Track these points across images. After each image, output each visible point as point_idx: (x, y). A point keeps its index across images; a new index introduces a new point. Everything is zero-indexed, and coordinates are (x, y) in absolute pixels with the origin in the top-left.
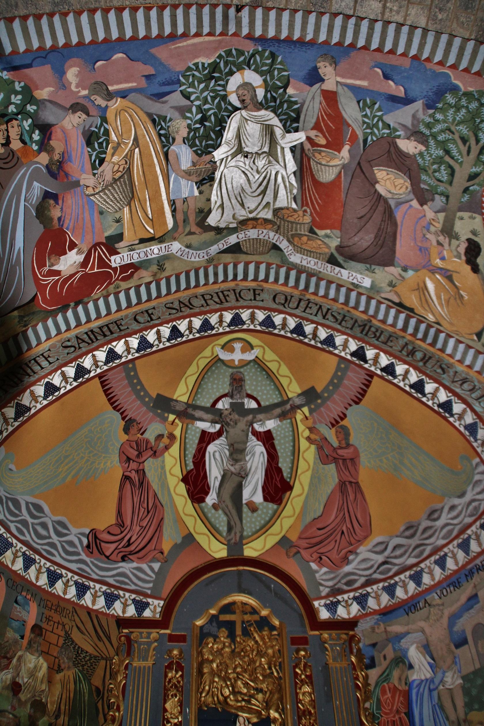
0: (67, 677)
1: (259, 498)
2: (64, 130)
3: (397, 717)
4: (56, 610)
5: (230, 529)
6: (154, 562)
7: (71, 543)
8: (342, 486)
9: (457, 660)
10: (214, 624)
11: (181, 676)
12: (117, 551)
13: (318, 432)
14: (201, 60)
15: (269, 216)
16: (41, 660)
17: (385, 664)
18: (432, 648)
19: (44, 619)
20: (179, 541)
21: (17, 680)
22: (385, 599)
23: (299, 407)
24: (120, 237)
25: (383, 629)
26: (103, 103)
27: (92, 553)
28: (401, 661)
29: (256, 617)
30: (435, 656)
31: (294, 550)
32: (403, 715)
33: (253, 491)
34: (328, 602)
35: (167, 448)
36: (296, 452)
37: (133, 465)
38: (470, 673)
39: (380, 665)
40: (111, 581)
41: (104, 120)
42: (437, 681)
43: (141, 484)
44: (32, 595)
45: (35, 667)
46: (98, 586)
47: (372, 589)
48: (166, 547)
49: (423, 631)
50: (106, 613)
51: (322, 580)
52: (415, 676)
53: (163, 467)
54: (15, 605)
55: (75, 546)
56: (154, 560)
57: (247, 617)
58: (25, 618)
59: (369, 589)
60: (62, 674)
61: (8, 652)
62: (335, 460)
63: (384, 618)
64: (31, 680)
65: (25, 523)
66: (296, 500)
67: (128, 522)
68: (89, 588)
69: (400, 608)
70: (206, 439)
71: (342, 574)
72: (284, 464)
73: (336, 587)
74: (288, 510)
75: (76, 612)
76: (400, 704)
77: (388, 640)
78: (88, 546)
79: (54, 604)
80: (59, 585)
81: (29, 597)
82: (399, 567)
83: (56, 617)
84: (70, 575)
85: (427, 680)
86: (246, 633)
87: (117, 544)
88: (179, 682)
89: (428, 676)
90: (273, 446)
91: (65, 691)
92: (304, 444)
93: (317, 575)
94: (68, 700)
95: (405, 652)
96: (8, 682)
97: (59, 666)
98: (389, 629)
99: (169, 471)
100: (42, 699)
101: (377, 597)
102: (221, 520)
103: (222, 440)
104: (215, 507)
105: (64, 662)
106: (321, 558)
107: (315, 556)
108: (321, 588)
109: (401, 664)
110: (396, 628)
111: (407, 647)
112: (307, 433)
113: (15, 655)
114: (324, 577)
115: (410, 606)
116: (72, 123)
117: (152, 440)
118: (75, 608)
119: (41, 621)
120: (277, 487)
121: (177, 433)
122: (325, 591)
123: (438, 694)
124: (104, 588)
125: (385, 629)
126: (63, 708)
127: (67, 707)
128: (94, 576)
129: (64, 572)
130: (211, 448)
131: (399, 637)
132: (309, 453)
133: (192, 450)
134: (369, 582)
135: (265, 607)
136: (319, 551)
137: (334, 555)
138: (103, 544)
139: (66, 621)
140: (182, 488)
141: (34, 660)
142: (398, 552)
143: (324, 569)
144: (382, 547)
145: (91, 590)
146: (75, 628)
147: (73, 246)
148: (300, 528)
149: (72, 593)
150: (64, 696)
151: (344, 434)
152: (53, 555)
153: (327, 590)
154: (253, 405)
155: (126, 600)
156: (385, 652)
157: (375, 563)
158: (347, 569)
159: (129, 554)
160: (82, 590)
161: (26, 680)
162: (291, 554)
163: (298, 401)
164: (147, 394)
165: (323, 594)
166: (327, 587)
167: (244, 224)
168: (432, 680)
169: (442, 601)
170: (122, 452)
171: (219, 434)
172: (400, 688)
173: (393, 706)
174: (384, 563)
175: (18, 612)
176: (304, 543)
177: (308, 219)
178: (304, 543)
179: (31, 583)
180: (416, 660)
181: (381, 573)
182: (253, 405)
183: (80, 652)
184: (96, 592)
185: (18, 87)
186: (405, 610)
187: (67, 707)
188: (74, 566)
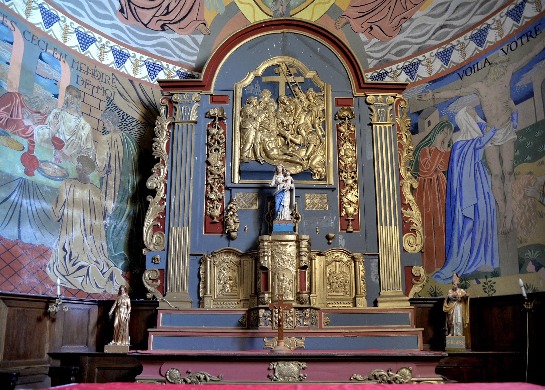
0: (114, 139)
3: (435, 176)
4: (93, 75)
6: (197, 34)
9: (515, 116)
10: (258, 86)
11: (224, 133)
12: (155, 19)
16: (83, 121)
17: (428, 130)
18: (485, 108)
19: (80, 82)
20: (222, 11)
21: (57, 135)
25: (431, 97)
27: (127, 18)
29: (301, 79)
30: (487, 116)
31: (343, 20)
32: (442, 173)
34: (375, 74)
38: (530, 127)
39: (424, 129)
40: (152, 50)
42: (484, 140)
44: (61, 55)
45: (77, 126)
46: (138, 55)
47: (424, 56)
48: (209, 17)
49: (477, 93)
50: (150, 83)
51: (371, 52)
54: (40, 61)
55: (106, 9)
56: (197, 31)
57: (291, 79)
58: (57, 78)
59: (420, 57)
60: (108, 136)
61: (41, 108)
63: (434, 85)
64: (74, 138)
68: (128, 56)
69: (453, 73)
71: (395, 42)
73: (385, 58)
75: (117, 80)
76: (439, 164)
77: (435, 106)
78: (122, 11)
79: (90, 69)
81: (58, 56)
82: (460, 28)
83: (95, 82)
84: (104, 40)
85: (473, 140)
86: (290, 93)
87: (154, 11)
88: (222, 138)
89: (476, 136)
91: (113, 151)
93: (366, 47)
94: (117, 159)
96: (47, 137)
97: (104, 128)
98: (437, 95)
100: (89, 156)
105: (109, 125)
106: (371, 28)
107: (366, 26)
108: (369, 60)
109: (446, 128)
111: (455, 111)
113: (50, 112)
114: (373, 49)
115: (466, 70)
118: (116, 76)
119: (77, 83)
122: (372, 63)
123: (484, 151)
124: (145, 58)
125: (433, 95)
126: (113, 165)
127: (117, 165)
128: (133, 45)
129: (97, 36)
131: (448, 102)
134: (421, 51)
135: (311, 70)
136: (369, 21)
137: (386, 25)
138: (137, 9)
139: (106, 86)
141: (74, 120)
142: (461, 12)
143: (375, 40)
145: (132, 59)
146: (117, 94)
149: (109, 59)
150: (113, 155)
152: (80, 15)
153: (375, 62)
155: (170, 71)
156: (430, 118)
157: (432, 28)
158: (399, 38)
159: (169, 23)
160: (121, 58)
161: (68, 137)
162: (340, 25)
165: (370, 67)
166: (376, 59)
168: (479, 140)
169: (507, 56)
172: (442, 150)
173: (431, 167)
174: (442, 27)
175: (45, 69)
176: (354, 13)
179: (56, 41)
180: (464, 122)
181: (436, 39)
183: (125, 117)
184: (137, 61)
186: (458, 74)
187: (117, 165)
188: (108, 31)
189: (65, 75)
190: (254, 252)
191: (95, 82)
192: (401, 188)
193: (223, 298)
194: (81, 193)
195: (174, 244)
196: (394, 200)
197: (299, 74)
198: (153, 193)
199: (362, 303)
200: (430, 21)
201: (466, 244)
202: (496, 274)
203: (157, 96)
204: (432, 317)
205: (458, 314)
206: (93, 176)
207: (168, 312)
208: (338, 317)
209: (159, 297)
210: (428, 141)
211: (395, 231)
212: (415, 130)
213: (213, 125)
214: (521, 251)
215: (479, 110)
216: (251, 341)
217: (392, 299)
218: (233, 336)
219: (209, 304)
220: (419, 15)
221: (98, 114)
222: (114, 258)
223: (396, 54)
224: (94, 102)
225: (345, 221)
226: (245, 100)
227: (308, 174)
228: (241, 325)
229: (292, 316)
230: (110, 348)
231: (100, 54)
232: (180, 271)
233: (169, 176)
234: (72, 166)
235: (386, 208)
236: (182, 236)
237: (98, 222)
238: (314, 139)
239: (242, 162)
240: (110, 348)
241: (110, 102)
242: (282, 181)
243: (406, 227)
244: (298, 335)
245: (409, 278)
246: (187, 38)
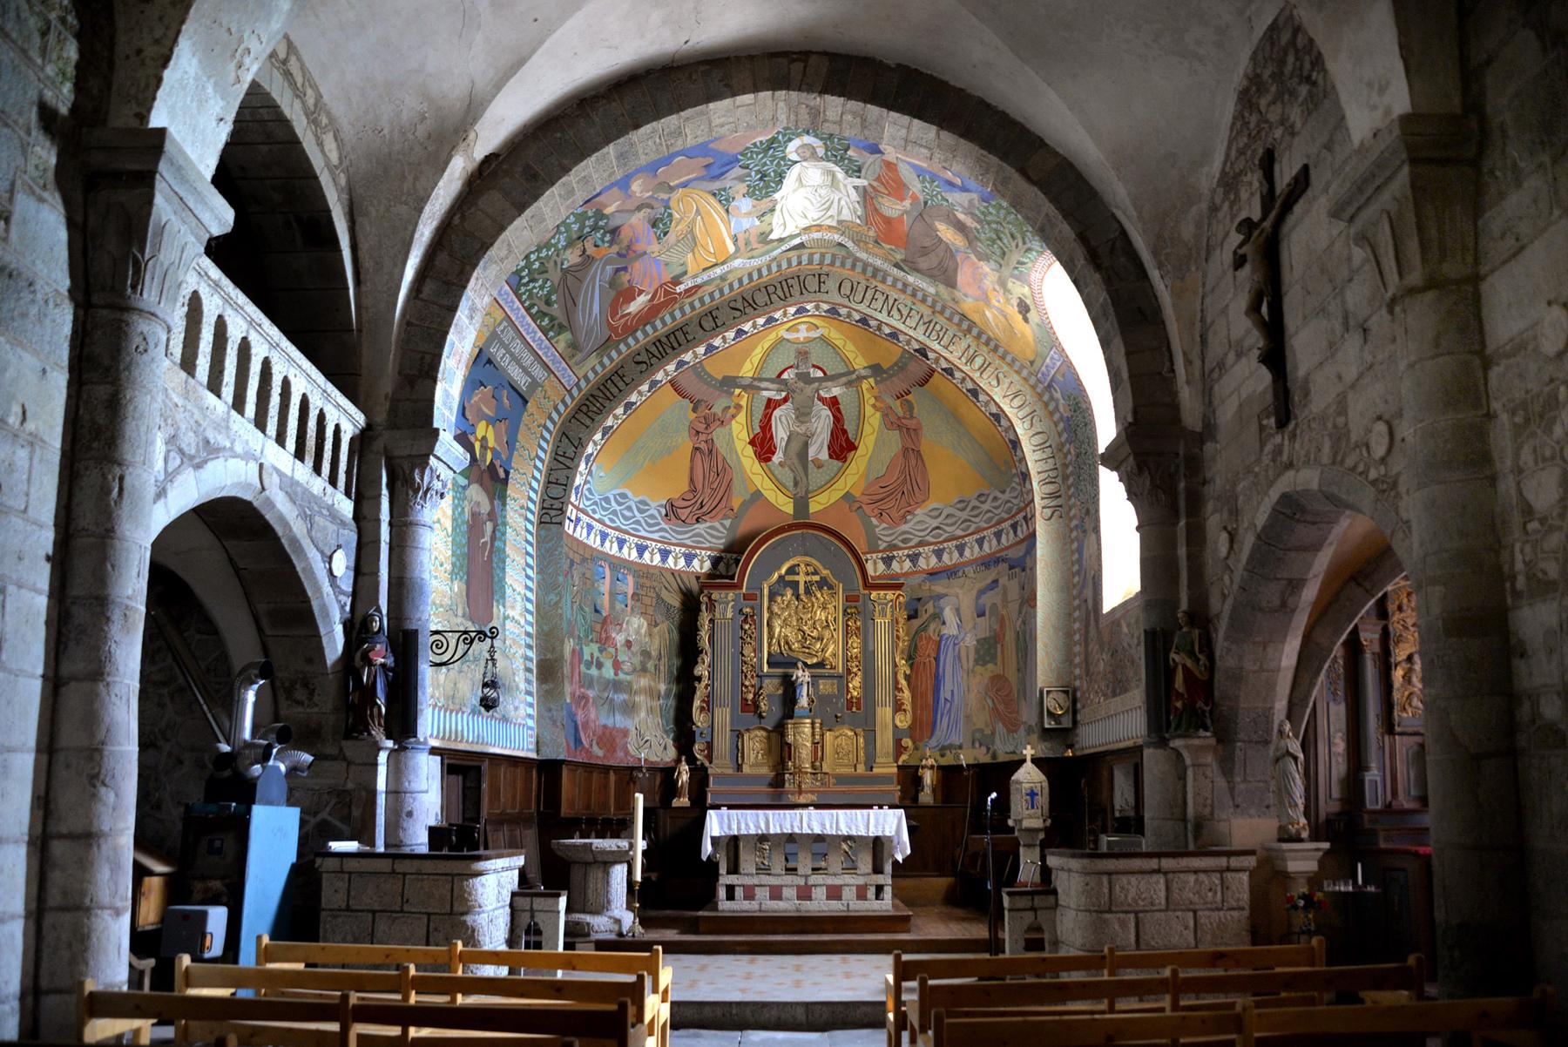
1: (824, 455)
2: (631, 226)
5: (796, 484)
7: (652, 517)
8: (905, 450)
13: (884, 402)
14: (757, 140)
15: (834, 224)
17: (925, 617)
20: (748, 497)
22: (933, 560)
23: (865, 378)
24: (685, 273)
26: (665, 197)
28: (937, 616)
29: (817, 578)
33: (819, 450)
35: (734, 416)
36: (861, 417)
37: (703, 437)
40: (688, 542)
41: (667, 207)
43: (710, 452)
48: (736, 503)
52: (945, 631)
53: (730, 434)
56: (725, 517)
62: (899, 427)
65: (614, 513)
66: (859, 463)
67: (699, 487)
70: (771, 405)
72: (849, 426)
74: (853, 468)
80: (647, 555)
83: (648, 583)
86: (808, 592)
90: (839, 410)
92: (869, 410)
95: (942, 610)
99: (739, 432)
101: (927, 559)
102: (787, 476)
103: (789, 404)
104: (781, 464)
107: (877, 512)
110: (938, 588)
112: (872, 401)
115: (951, 572)
116: (638, 220)
117: (719, 413)
120: (842, 446)
121: (743, 403)
122: (883, 546)
130: (777, 413)
131: (940, 597)
132: (874, 420)
133: (758, 415)
134: (921, 544)
137: (894, 513)
140: (750, 450)
142: (949, 521)
144: (935, 513)
147: (641, 292)
148: (863, 486)
151: (910, 407)
154: (820, 374)
158: (904, 527)
160: (665, 554)
163: (864, 373)
164: (713, 378)
167: (807, 229)
170: (691, 428)
171: (785, 400)
176: (866, 499)
177: (872, 233)
178: (866, 499)
182: (820, 374)
185: (590, 214)
189: (629, 586)
190: (780, 729)
191: (648, 583)
192: (895, 674)
193: (756, 765)
194: (644, 682)
195: (716, 721)
196: (889, 684)
197: (816, 573)
198: (699, 679)
199: (861, 769)
200: (928, 520)
201: (945, 720)
202: (960, 747)
203: (695, 586)
204: (910, 778)
205: (928, 777)
206: (650, 665)
207: (716, 776)
208: (841, 779)
209: (707, 764)
210: (924, 628)
211: (889, 710)
212: (913, 616)
213: (745, 621)
214: (974, 732)
215: (958, 611)
216: (780, 796)
217: (884, 765)
218: (768, 793)
219: (746, 769)
220: (920, 512)
221: (650, 610)
222: (666, 732)
223: (904, 541)
224: (647, 601)
225: (850, 704)
226: (772, 599)
227: (821, 665)
228: (771, 785)
229: (808, 779)
230: (676, 803)
231: (652, 559)
232: (723, 743)
233: (712, 665)
234: (637, 660)
235: (883, 693)
236: (723, 716)
237: (656, 704)
238: (827, 634)
239: (769, 654)
240: (676, 803)
241: (658, 596)
242: (802, 675)
243: (898, 707)
244: (812, 792)
245: (899, 749)
246: (717, 524)
